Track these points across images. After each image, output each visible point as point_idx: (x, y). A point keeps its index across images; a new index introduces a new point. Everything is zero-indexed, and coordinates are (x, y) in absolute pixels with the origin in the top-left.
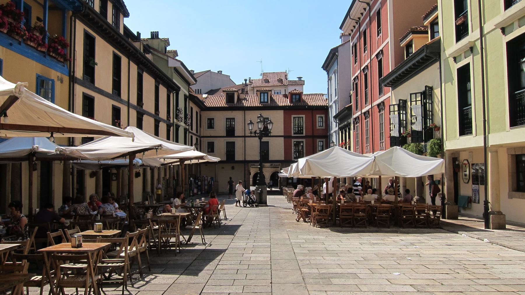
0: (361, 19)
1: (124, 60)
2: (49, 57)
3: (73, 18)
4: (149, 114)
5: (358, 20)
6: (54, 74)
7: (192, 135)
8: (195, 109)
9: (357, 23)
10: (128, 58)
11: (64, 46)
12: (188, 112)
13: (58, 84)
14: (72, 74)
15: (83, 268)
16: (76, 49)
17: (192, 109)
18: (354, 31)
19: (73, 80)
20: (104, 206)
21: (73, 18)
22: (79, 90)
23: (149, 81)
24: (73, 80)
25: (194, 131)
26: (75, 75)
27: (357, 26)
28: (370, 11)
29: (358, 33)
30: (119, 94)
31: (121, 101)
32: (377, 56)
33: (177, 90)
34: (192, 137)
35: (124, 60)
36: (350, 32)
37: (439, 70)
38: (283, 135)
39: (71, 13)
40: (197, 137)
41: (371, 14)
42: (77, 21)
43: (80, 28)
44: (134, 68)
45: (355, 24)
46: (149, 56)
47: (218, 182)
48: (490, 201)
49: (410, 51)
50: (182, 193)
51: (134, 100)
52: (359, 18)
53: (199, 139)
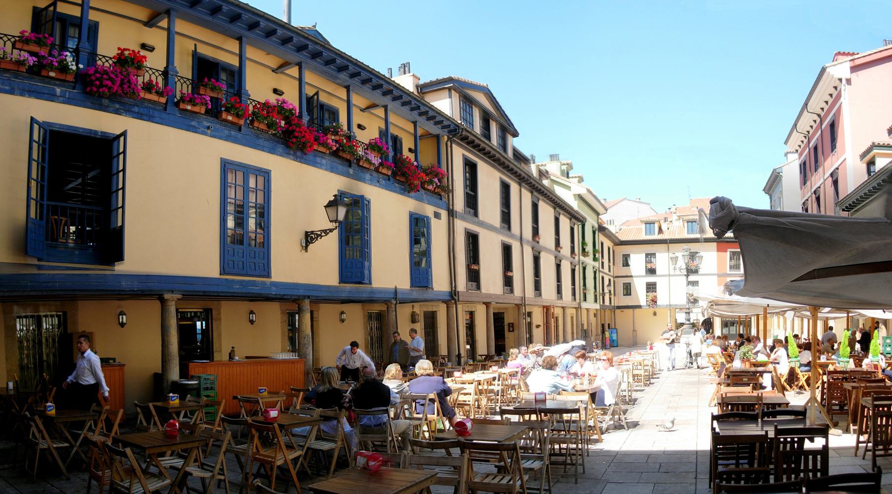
0: (811, 133)
1: (514, 187)
2: (423, 190)
3: (449, 143)
4: (548, 251)
5: (807, 133)
6: (429, 210)
7: (603, 275)
8: (607, 243)
9: (805, 137)
10: (520, 185)
11: (439, 175)
12: (597, 248)
13: (434, 222)
14: (451, 207)
15: (606, 231)
16: (454, 178)
17: (602, 244)
18: (802, 146)
19: (451, 213)
20: (239, 431)
21: (449, 143)
22: (461, 226)
23: (546, 212)
24: (451, 213)
25: (606, 270)
26: (455, 209)
27: (806, 141)
28: (821, 123)
29: (807, 150)
30: (509, 228)
31: (513, 236)
32: (832, 175)
33: (582, 222)
34: (610, 271)
35: (514, 187)
36: (798, 148)
37: (624, 310)
38: (716, 272)
39: (446, 138)
40: (610, 277)
41: (823, 126)
42: (454, 145)
43: (459, 154)
44: (527, 197)
45: (803, 139)
46: (546, 182)
47: (636, 331)
48: (462, 355)
49: (872, 169)
50: (474, 361)
51: (528, 234)
52: (808, 132)
53: (612, 280)
